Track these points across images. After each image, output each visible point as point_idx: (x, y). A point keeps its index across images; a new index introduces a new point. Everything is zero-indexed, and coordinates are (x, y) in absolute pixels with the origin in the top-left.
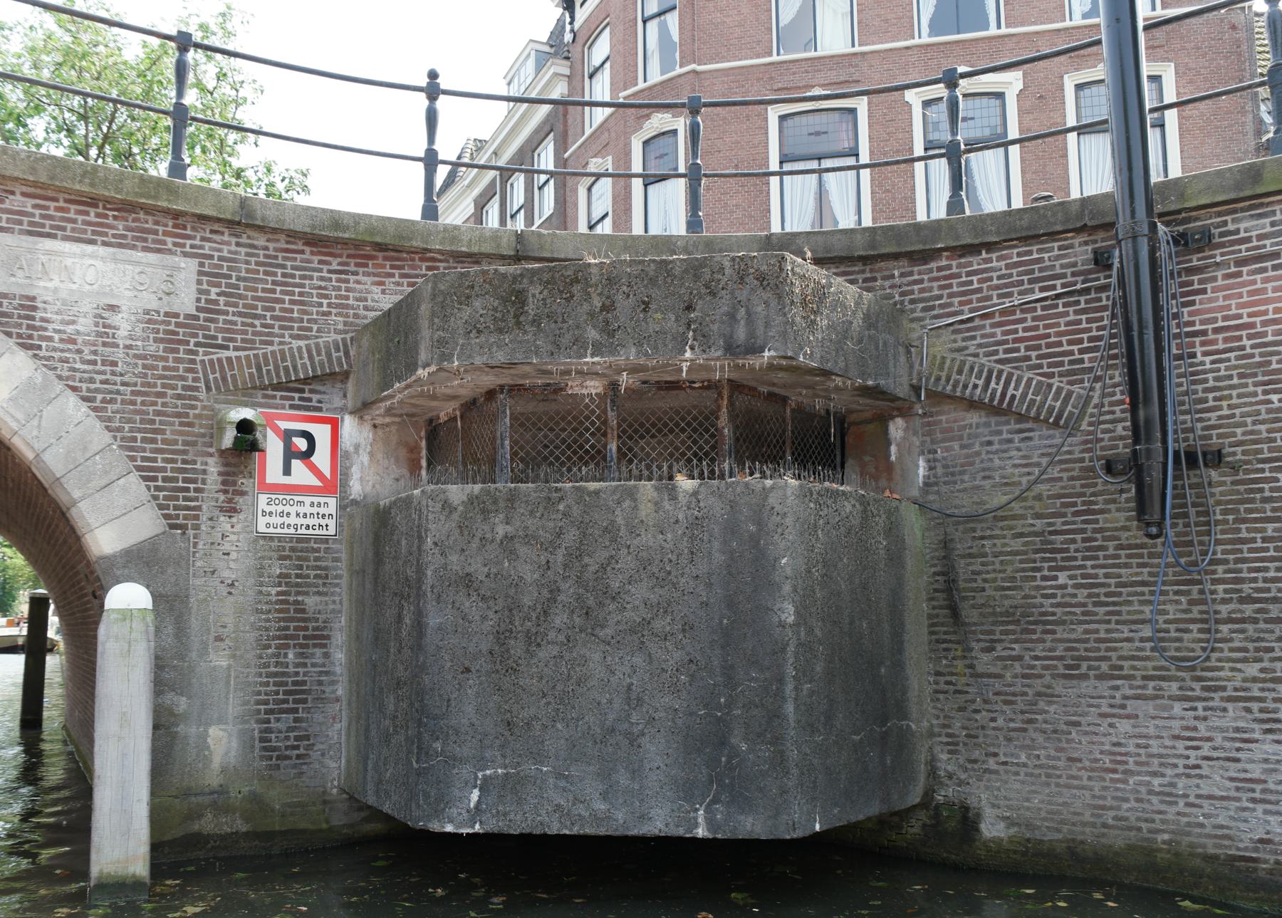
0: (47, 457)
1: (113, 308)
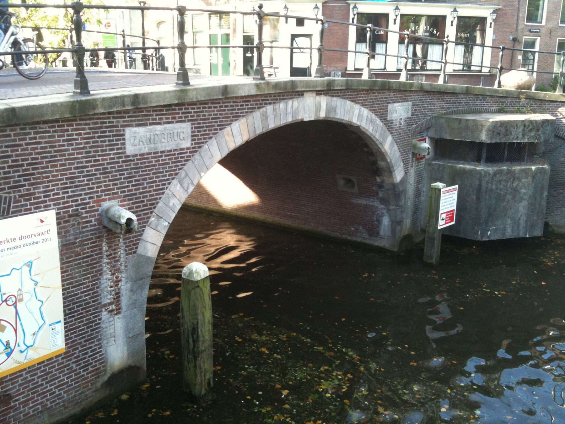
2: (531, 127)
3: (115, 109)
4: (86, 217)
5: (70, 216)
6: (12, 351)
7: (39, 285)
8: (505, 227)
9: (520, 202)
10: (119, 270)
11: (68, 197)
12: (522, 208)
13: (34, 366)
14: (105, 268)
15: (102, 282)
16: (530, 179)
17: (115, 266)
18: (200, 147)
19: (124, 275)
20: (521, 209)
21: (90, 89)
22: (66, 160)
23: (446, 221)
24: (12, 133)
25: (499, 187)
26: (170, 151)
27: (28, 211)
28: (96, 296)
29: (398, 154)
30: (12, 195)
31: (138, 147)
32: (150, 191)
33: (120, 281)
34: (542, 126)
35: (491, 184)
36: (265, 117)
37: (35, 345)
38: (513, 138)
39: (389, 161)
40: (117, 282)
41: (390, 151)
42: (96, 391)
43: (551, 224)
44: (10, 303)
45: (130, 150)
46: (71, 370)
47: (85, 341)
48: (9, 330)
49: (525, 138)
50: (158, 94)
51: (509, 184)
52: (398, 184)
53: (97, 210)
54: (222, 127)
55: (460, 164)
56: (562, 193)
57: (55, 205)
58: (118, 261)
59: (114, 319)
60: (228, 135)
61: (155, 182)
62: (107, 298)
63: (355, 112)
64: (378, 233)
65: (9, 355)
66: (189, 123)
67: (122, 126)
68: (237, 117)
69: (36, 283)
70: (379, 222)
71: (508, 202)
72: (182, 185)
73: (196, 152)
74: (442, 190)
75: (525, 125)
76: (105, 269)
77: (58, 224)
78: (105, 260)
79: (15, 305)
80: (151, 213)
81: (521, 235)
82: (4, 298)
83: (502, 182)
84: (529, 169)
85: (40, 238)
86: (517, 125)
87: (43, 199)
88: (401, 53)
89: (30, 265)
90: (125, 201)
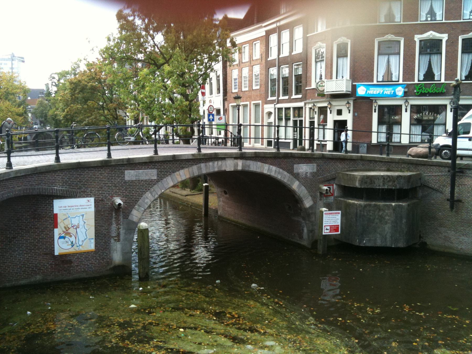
0: (301, 195)
1: (307, 173)
2: (388, 179)
3: (119, 163)
4: (106, 202)
5: (100, 201)
6: (74, 245)
7: (86, 223)
8: (376, 239)
9: (386, 224)
10: (119, 224)
11: (100, 194)
12: (387, 228)
13: (82, 253)
14: (114, 222)
15: (112, 227)
16: (391, 211)
17: (118, 222)
18: (162, 179)
19: (122, 227)
20: (386, 228)
21: (112, 156)
22: (100, 180)
23: (330, 231)
24: (80, 170)
25: (369, 214)
26: (146, 180)
27: (84, 197)
28: (109, 232)
29: (306, 192)
30: (78, 191)
31: (130, 178)
32: (135, 195)
33: (120, 228)
34: (397, 179)
35: (363, 212)
36: (200, 169)
37: (83, 245)
38: (376, 186)
39: (298, 195)
40: (119, 229)
41: (297, 190)
42: (107, 270)
43: (428, 243)
44: (74, 228)
45: (127, 178)
46: (97, 259)
47: (104, 249)
48: (73, 237)
49: (385, 186)
50: (139, 158)
51: (376, 213)
52: (307, 208)
53: (111, 200)
54: (174, 172)
55: (349, 200)
56: (433, 223)
57: (94, 196)
58: (120, 220)
59: (116, 244)
60: (177, 175)
61: (138, 192)
62: (114, 234)
63: (265, 168)
64: (303, 237)
65: (72, 246)
66: (156, 170)
67: (123, 170)
68: (183, 168)
69: (85, 223)
70: (303, 230)
71: (377, 223)
72: (151, 194)
73: (159, 181)
74: (324, 212)
75: (384, 178)
76: (113, 223)
77: (95, 203)
78: (114, 219)
79: (76, 229)
80: (136, 204)
81: (388, 244)
82: (72, 225)
83: (371, 212)
84: (390, 205)
85: (88, 207)
86: (378, 178)
87: (89, 193)
88: (413, 131)
89: (83, 216)
90: (123, 198)
